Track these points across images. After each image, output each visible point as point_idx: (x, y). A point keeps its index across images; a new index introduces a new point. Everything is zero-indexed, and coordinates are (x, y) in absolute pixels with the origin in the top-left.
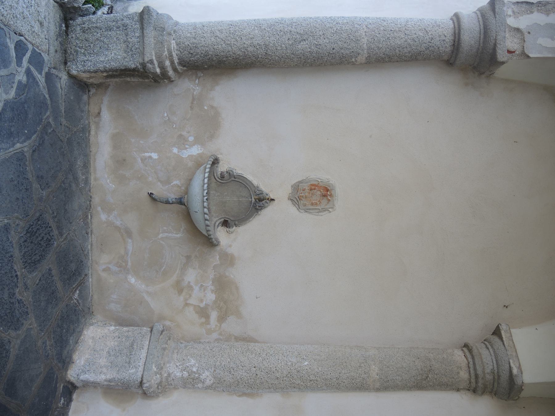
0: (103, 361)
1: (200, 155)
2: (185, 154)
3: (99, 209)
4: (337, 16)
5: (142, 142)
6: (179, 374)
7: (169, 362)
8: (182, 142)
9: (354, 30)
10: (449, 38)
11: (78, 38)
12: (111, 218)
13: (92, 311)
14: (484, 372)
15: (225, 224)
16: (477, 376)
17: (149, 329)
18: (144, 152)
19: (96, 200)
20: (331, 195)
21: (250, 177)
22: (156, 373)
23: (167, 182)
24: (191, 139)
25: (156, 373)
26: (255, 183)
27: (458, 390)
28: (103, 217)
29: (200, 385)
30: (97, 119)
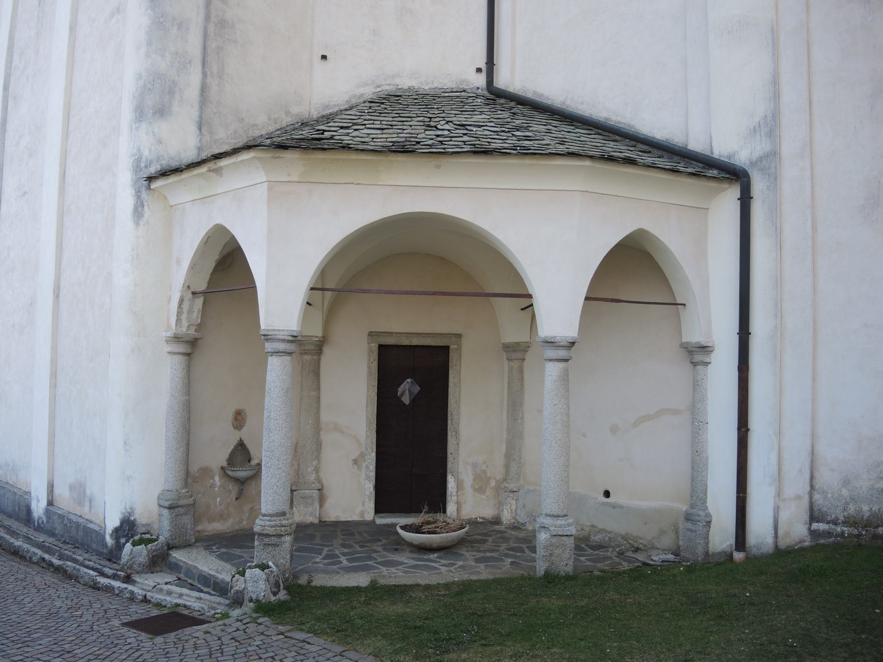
0: (310, 509)
1: (219, 476)
2: (218, 484)
3: (241, 525)
4: (708, 499)
5: (212, 507)
6: (314, 475)
7: (310, 480)
8: (213, 486)
9: (182, 403)
10: (184, 357)
11: (179, 541)
12: (245, 518)
13: (359, 468)
14: (315, 350)
15: (249, 461)
16: (317, 353)
17: (294, 492)
18: (216, 505)
19: (237, 527)
20: (240, 411)
21: (230, 450)
22: (315, 484)
23: (230, 491)
24: (212, 481)
25: (315, 484)
26: (232, 447)
27: (320, 359)
28: (245, 522)
29: (318, 465)
30: (201, 532)
